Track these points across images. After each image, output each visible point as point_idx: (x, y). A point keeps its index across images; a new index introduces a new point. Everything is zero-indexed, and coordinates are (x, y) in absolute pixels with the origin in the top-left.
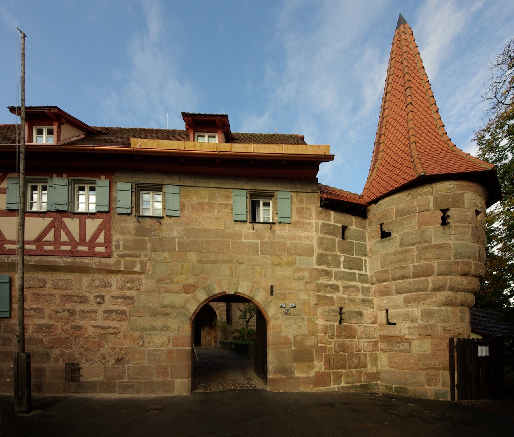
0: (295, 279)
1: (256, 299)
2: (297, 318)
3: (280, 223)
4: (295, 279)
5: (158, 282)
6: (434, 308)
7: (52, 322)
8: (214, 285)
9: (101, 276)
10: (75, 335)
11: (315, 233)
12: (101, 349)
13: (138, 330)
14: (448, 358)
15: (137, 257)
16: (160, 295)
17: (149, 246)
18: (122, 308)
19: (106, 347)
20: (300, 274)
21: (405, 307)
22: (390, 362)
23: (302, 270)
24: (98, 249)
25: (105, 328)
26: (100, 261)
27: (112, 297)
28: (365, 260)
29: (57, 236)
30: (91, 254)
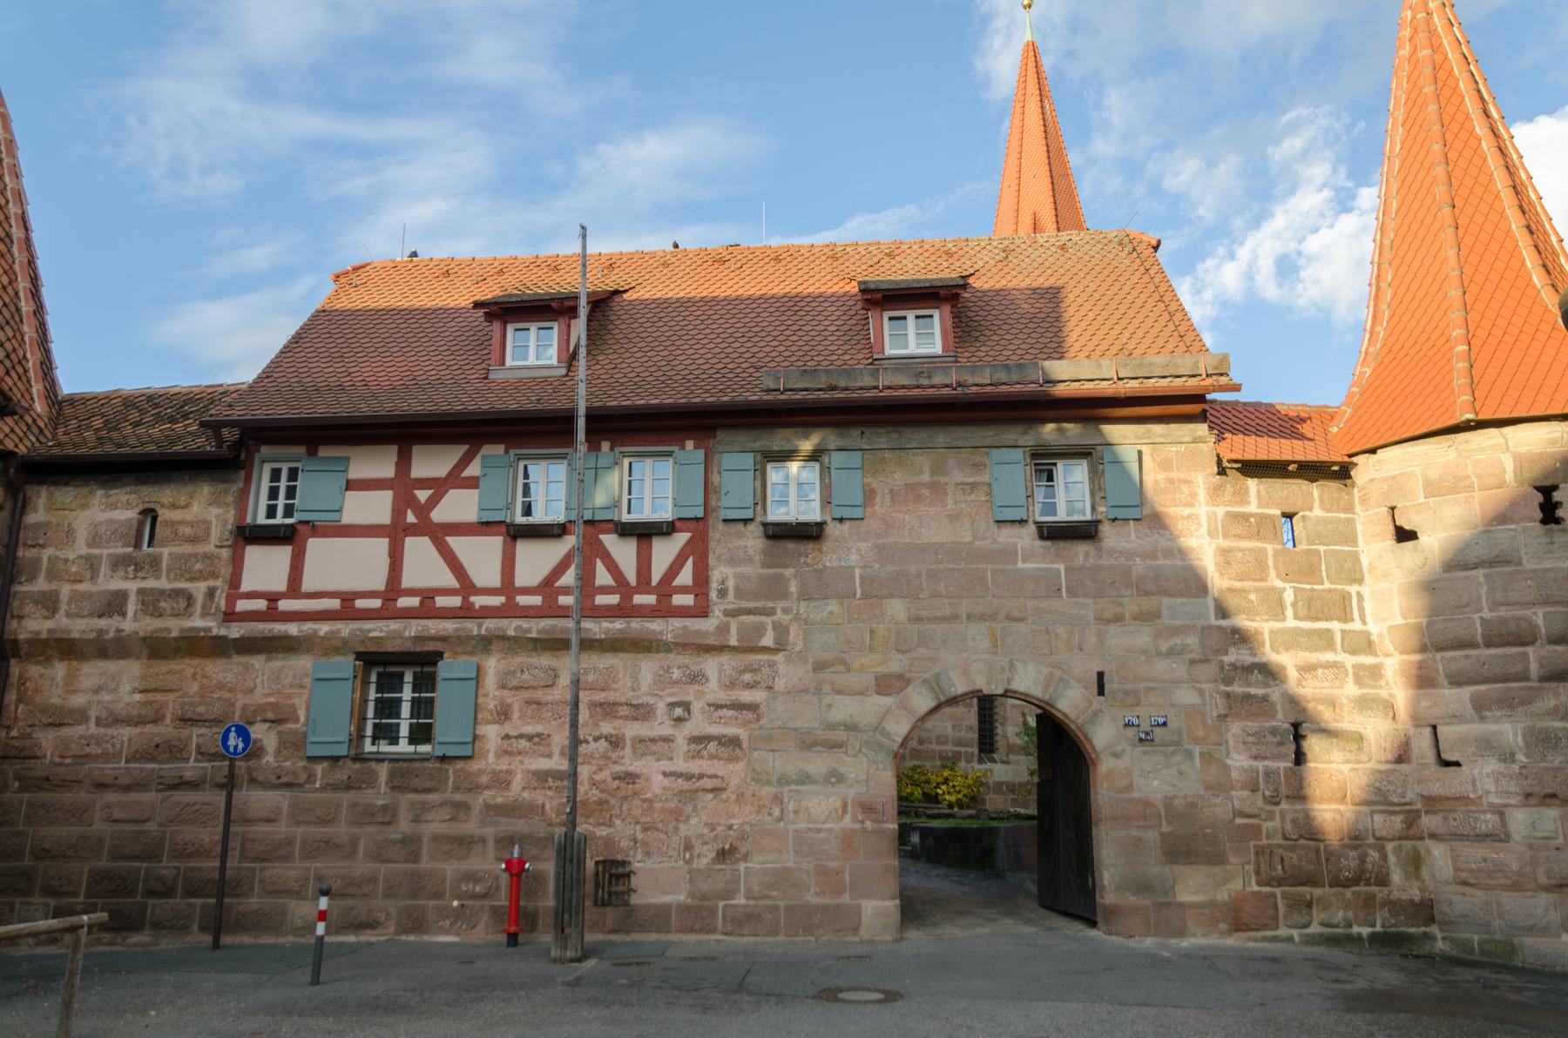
0: (1159, 654)
1: (1060, 706)
2: (1173, 753)
3: (1114, 520)
4: (1159, 654)
5: (815, 670)
8: (951, 674)
9: (685, 659)
10: (622, 794)
11: (1207, 540)
12: (682, 827)
13: (769, 783)
15: (767, 614)
16: (820, 701)
17: (793, 589)
18: (732, 731)
19: (694, 821)
20: (1177, 641)
21: (1476, 717)
24: (680, 600)
25: (693, 776)
26: (685, 627)
28: (1359, 594)
29: (587, 576)
30: (663, 610)
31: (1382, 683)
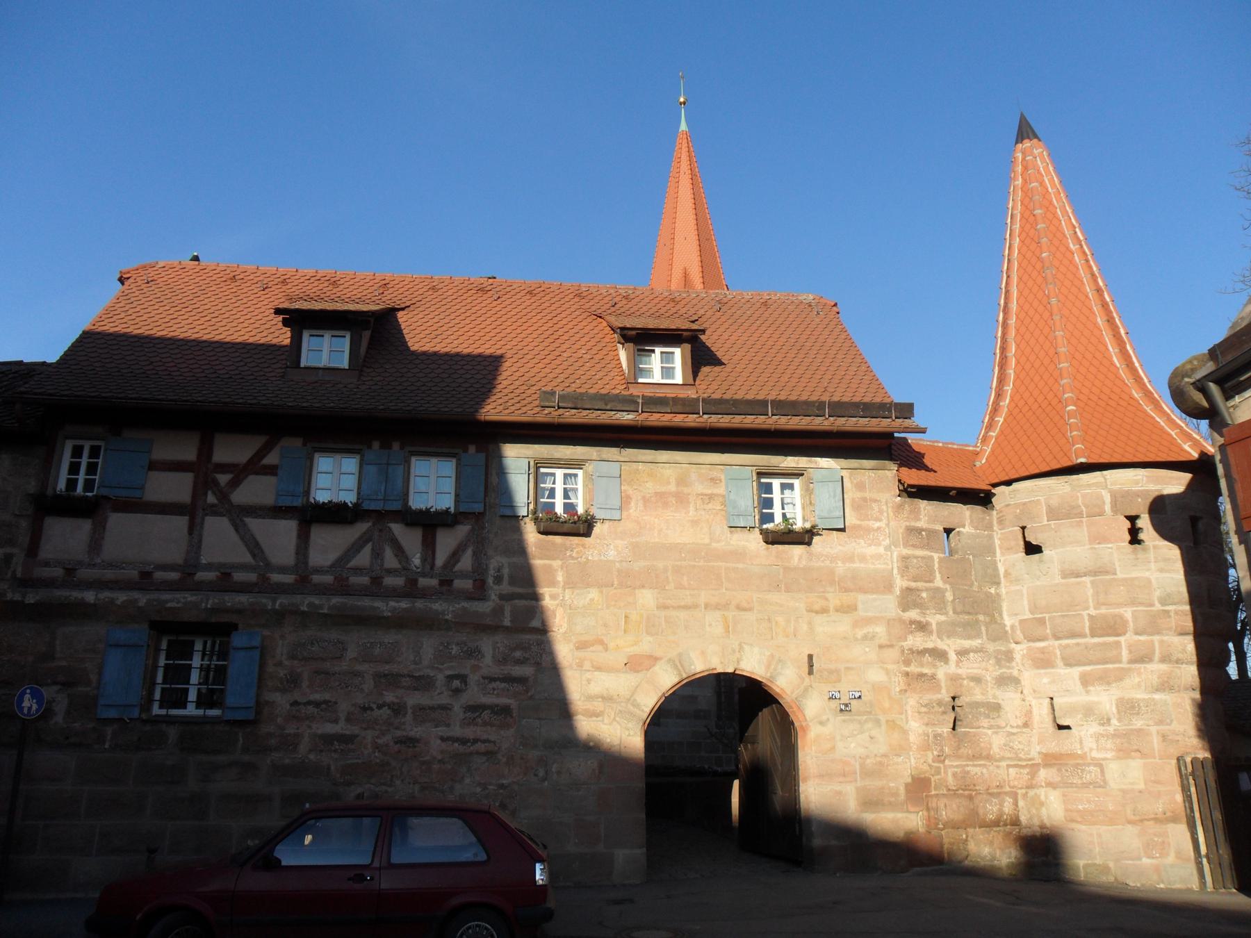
0: (856, 639)
1: (778, 683)
2: (866, 721)
6: (1139, 696)
7: (355, 730)
8: (692, 655)
14: (1179, 798)
18: (504, 701)
19: (467, 781)
22: (1067, 810)
23: (869, 621)
25: (468, 741)
27: (484, 678)
31: (1014, 664)
